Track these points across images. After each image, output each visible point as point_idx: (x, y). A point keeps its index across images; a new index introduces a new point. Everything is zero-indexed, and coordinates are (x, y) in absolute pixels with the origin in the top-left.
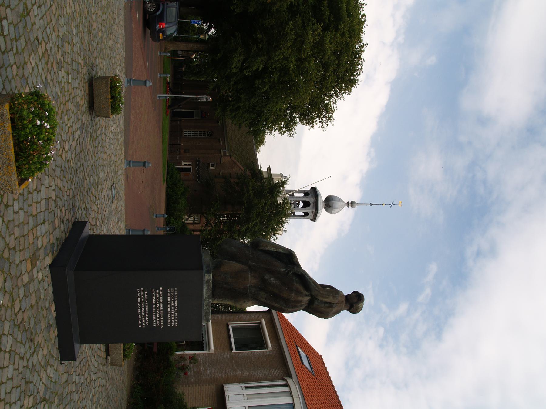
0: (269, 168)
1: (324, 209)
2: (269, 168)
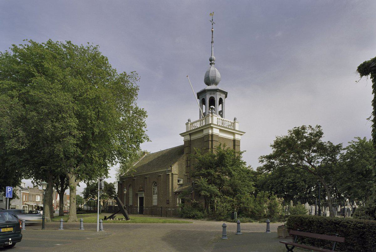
0: (182, 135)
2: (182, 135)
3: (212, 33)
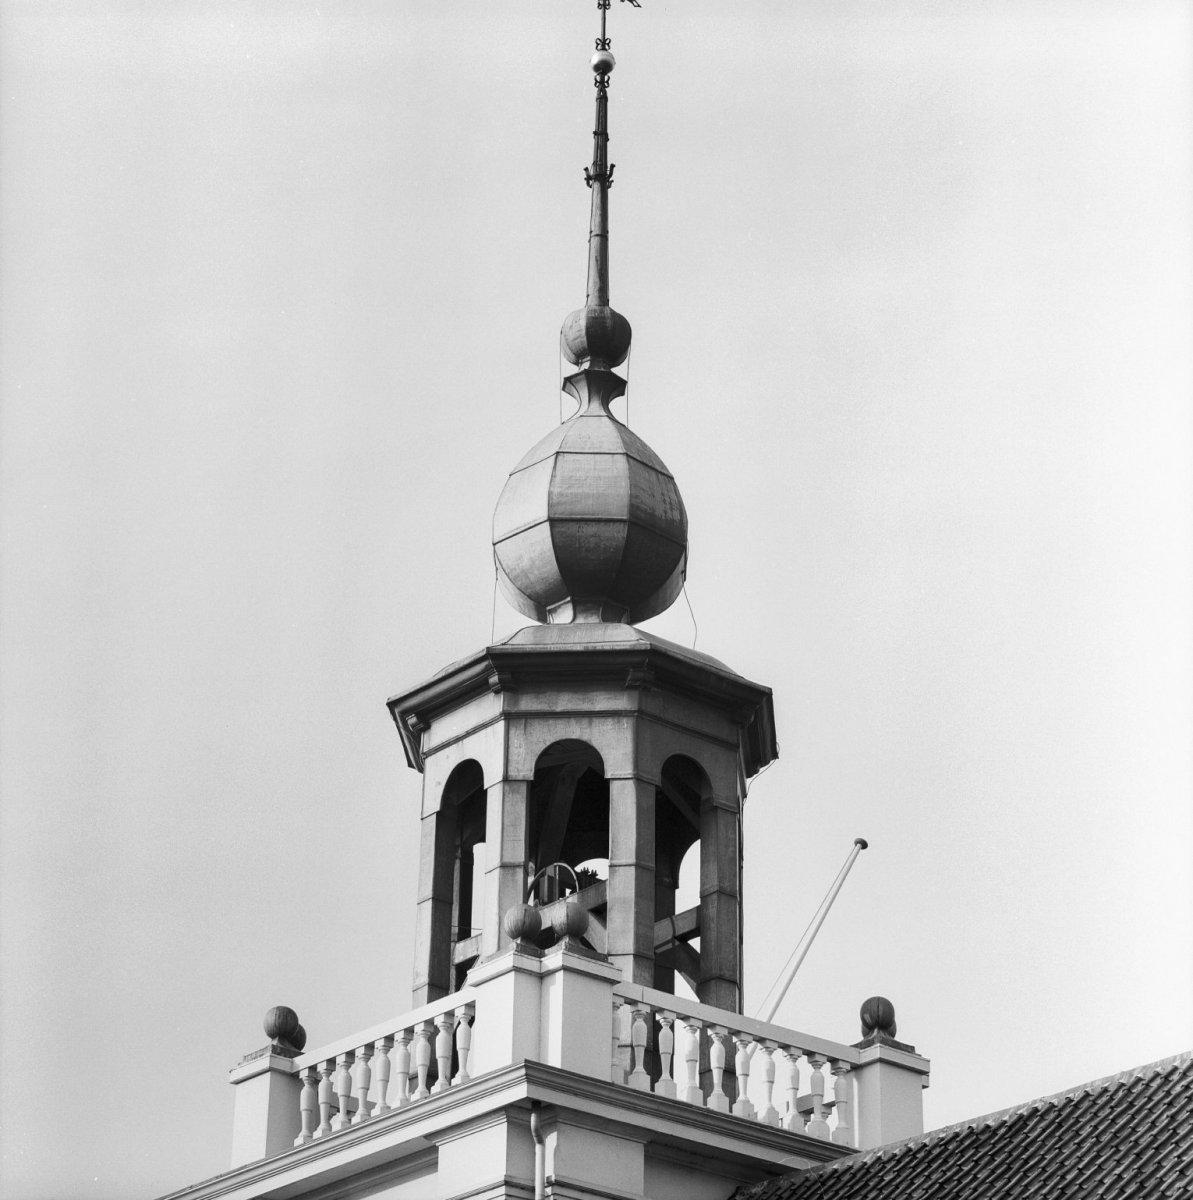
1: (642, 626)
3: (602, 85)
